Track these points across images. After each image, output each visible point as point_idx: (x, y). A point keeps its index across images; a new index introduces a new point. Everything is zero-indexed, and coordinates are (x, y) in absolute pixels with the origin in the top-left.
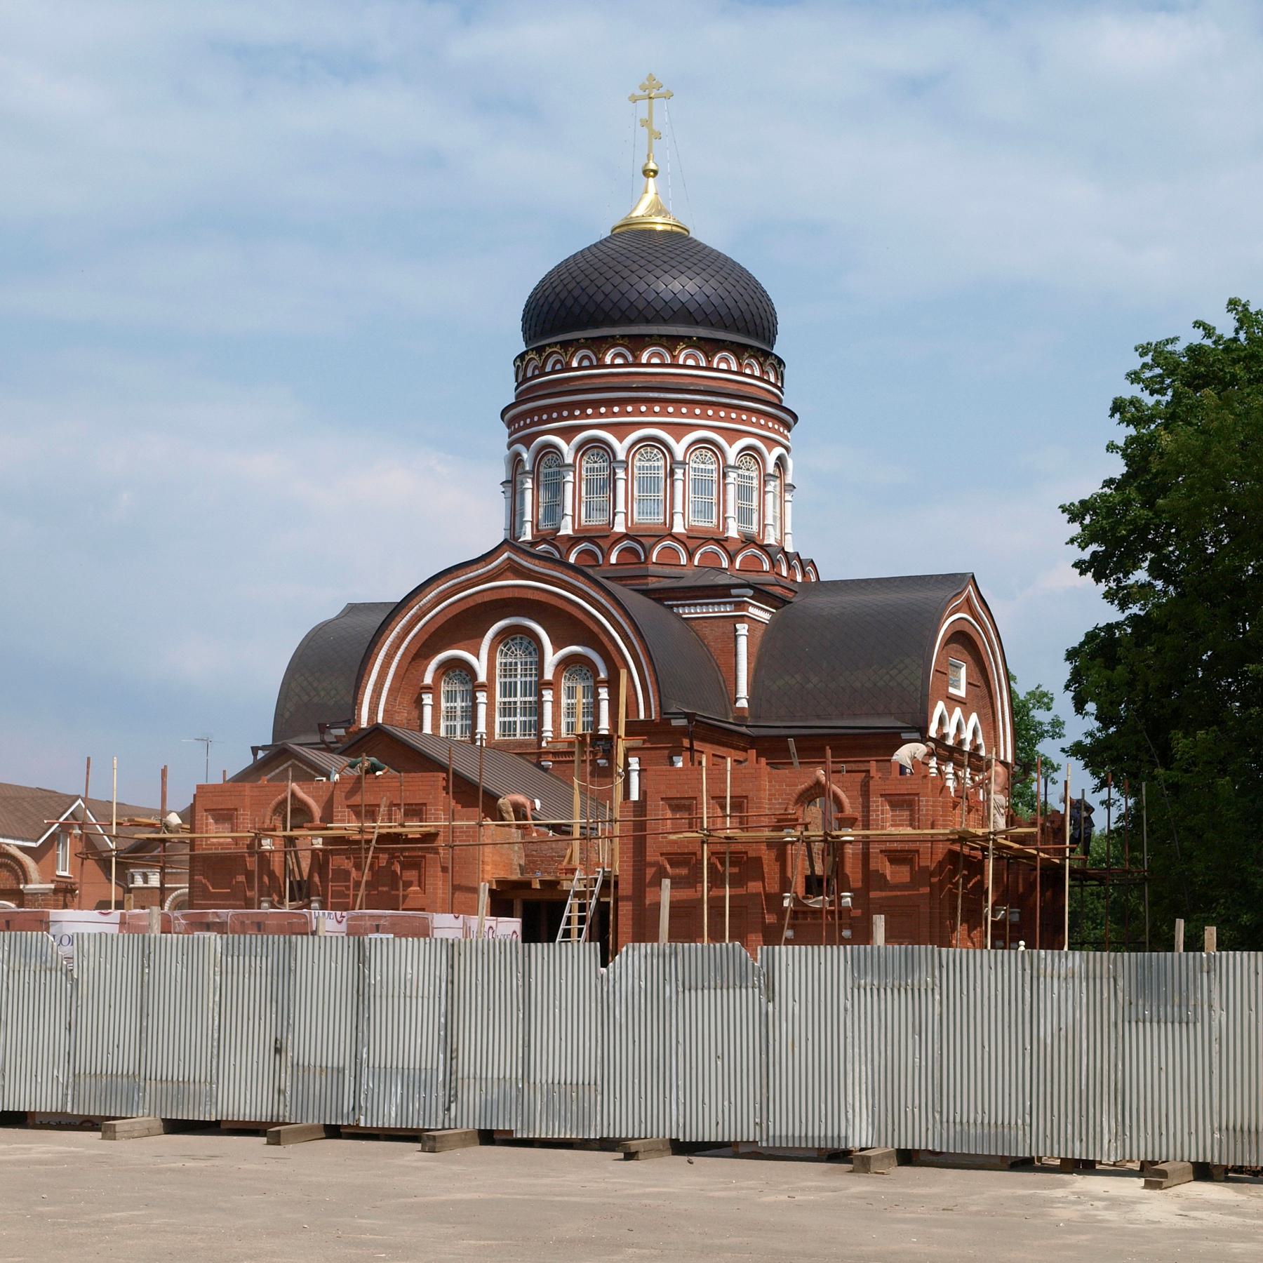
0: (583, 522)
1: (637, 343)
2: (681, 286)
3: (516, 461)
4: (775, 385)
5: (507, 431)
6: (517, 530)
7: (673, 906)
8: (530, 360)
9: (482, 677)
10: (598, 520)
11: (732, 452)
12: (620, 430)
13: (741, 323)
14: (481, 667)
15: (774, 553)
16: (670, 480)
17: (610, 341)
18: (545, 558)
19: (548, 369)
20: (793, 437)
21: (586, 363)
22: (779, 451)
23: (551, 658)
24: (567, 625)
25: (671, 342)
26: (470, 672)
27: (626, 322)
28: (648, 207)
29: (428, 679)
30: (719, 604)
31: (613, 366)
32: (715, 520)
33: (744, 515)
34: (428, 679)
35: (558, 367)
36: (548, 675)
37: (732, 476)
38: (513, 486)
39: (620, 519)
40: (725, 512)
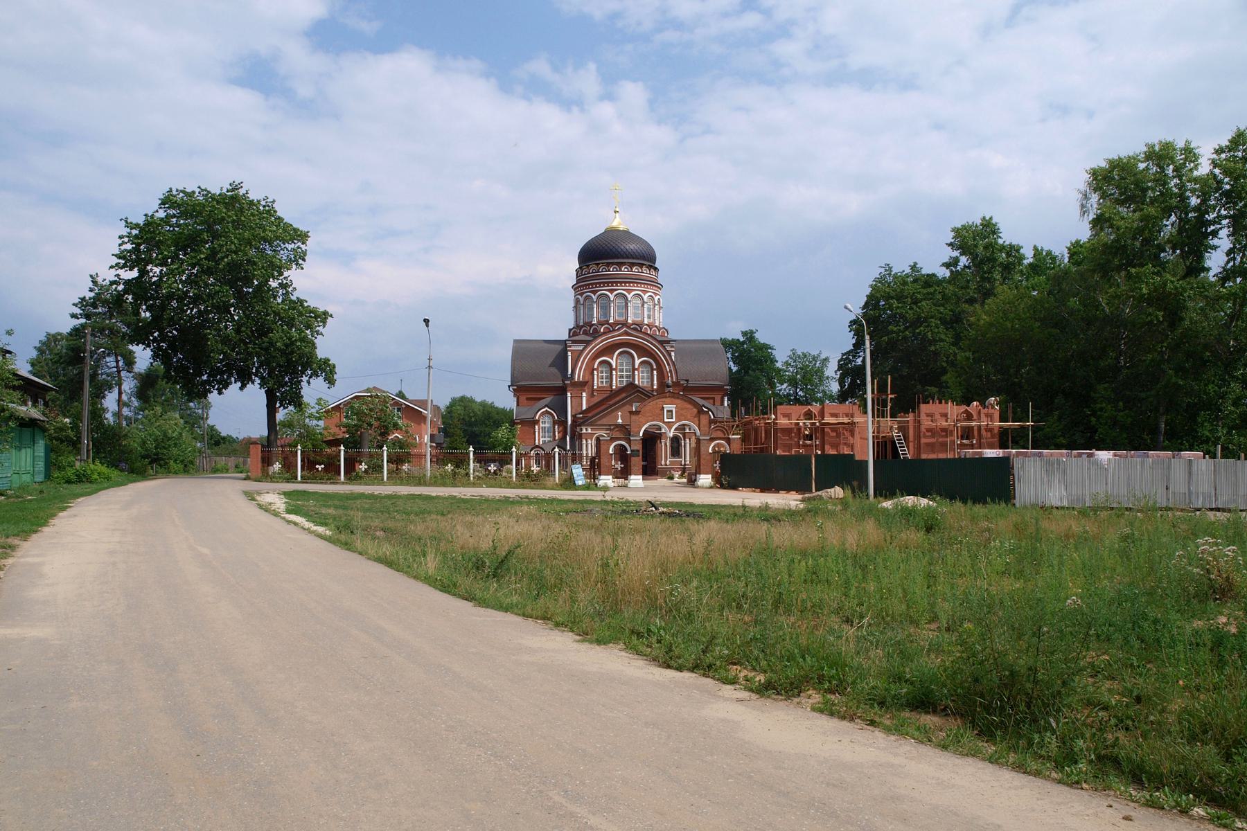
1: (632, 265)
2: (632, 247)
3: (577, 301)
7: (339, 474)
10: (622, 319)
11: (645, 297)
12: (611, 291)
13: (647, 258)
14: (614, 363)
15: (638, 327)
16: (639, 306)
17: (623, 264)
18: (635, 329)
23: (637, 362)
24: (643, 351)
25: (641, 265)
26: (609, 364)
27: (609, 259)
28: (618, 223)
33: (649, 317)
38: (576, 308)
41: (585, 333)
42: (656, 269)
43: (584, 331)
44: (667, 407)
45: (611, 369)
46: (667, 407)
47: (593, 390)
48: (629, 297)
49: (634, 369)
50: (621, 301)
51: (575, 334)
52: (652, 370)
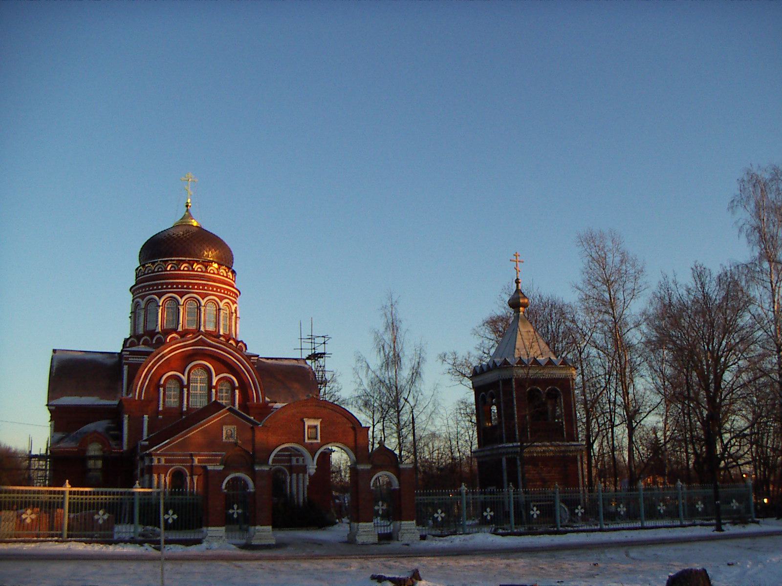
4: (232, 280)
5: (132, 296)
8: (141, 269)
19: (146, 272)
20: (238, 300)
22: (235, 305)
24: (225, 365)
26: (180, 380)
29: (162, 382)
31: (197, 271)
34: (162, 382)
35: (150, 271)
36: (214, 384)
37: (222, 312)
38: (134, 314)
39: (180, 325)
41: (146, 343)
42: (233, 272)
43: (144, 338)
44: (308, 423)
46: (308, 423)
51: (133, 344)
52: (233, 388)
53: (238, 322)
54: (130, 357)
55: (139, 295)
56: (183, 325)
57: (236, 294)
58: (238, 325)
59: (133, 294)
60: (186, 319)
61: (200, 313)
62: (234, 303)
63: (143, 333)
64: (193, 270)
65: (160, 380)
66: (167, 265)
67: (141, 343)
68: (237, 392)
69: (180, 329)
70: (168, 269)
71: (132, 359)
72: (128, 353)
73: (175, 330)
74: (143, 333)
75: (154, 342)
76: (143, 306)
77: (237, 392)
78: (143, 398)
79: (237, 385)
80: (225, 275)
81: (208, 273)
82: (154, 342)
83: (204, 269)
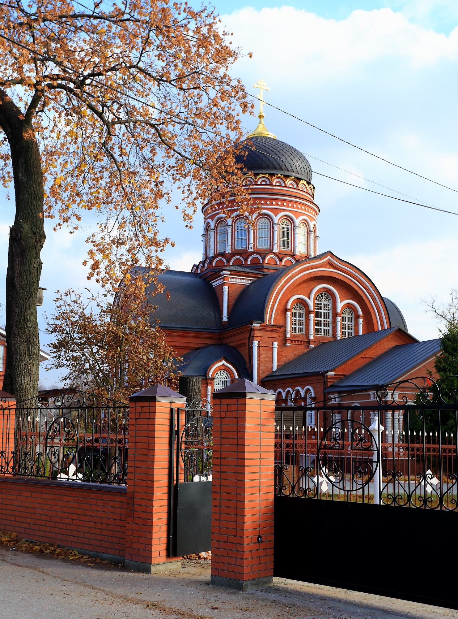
0: (258, 247)
6: (218, 250)
9: (312, 308)
11: (297, 221)
14: (311, 304)
21: (264, 183)
22: (314, 222)
23: (340, 305)
24: (349, 290)
30: (236, 278)
32: (269, 246)
36: (339, 311)
40: (273, 242)
45: (309, 312)
47: (285, 340)
48: (276, 219)
49: (336, 315)
50: (264, 224)
52: (358, 317)
53: (317, 242)
54: (231, 278)
55: (209, 216)
56: (254, 245)
57: (316, 212)
58: (317, 245)
59: (204, 215)
60: (290, 239)
61: (294, 234)
62: (312, 219)
63: (230, 252)
64: (271, 185)
65: (287, 303)
66: (257, 178)
67: (231, 264)
68: (361, 320)
69: (275, 250)
70: (259, 183)
71: (232, 280)
72: (229, 273)
73: (271, 251)
74: (230, 252)
75: (249, 263)
76: (213, 227)
77: (361, 320)
78: (225, 319)
79: (360, 313)
80: (295, 187)
81: (273, 185)
82: (249, 263)
83: (295, 187)
